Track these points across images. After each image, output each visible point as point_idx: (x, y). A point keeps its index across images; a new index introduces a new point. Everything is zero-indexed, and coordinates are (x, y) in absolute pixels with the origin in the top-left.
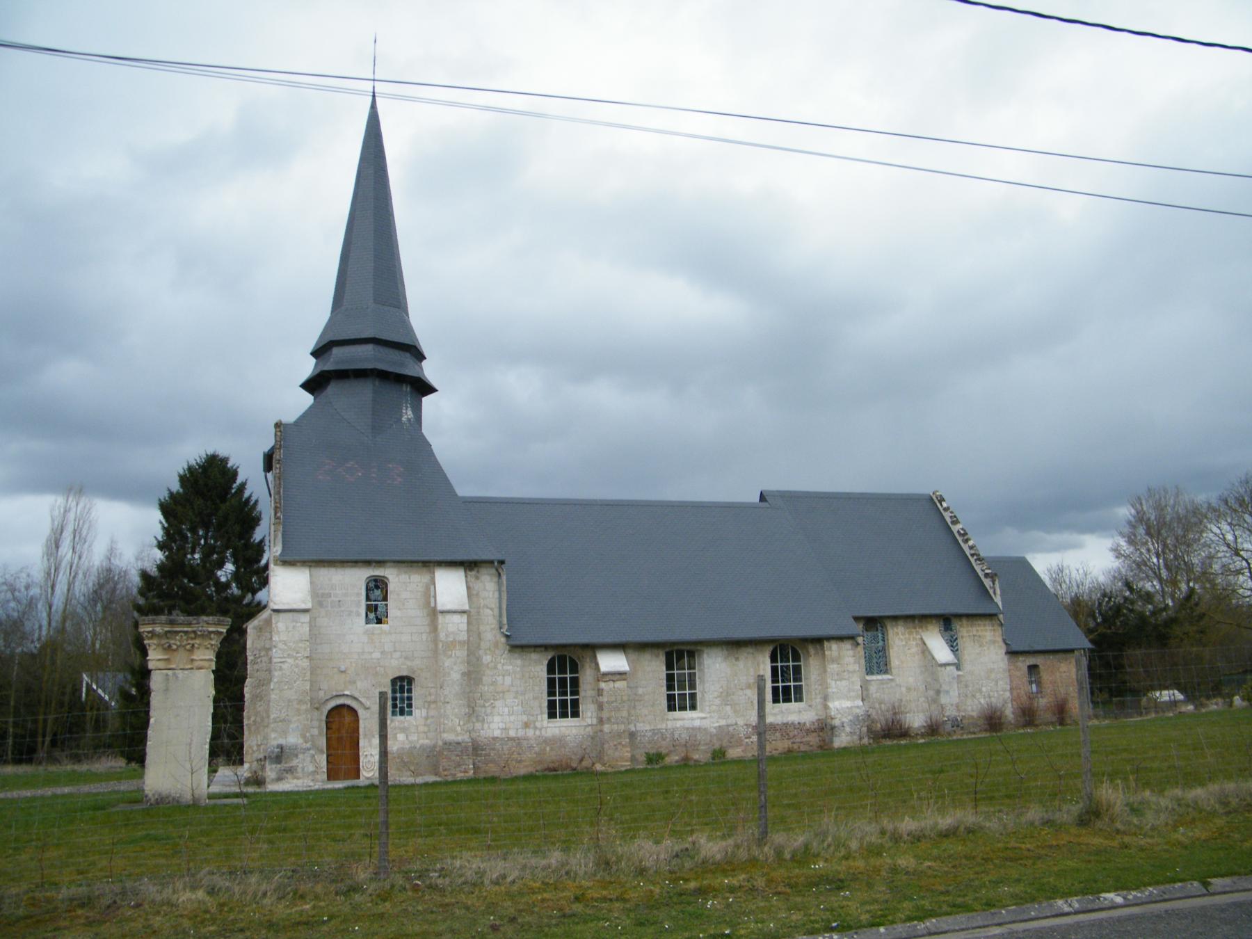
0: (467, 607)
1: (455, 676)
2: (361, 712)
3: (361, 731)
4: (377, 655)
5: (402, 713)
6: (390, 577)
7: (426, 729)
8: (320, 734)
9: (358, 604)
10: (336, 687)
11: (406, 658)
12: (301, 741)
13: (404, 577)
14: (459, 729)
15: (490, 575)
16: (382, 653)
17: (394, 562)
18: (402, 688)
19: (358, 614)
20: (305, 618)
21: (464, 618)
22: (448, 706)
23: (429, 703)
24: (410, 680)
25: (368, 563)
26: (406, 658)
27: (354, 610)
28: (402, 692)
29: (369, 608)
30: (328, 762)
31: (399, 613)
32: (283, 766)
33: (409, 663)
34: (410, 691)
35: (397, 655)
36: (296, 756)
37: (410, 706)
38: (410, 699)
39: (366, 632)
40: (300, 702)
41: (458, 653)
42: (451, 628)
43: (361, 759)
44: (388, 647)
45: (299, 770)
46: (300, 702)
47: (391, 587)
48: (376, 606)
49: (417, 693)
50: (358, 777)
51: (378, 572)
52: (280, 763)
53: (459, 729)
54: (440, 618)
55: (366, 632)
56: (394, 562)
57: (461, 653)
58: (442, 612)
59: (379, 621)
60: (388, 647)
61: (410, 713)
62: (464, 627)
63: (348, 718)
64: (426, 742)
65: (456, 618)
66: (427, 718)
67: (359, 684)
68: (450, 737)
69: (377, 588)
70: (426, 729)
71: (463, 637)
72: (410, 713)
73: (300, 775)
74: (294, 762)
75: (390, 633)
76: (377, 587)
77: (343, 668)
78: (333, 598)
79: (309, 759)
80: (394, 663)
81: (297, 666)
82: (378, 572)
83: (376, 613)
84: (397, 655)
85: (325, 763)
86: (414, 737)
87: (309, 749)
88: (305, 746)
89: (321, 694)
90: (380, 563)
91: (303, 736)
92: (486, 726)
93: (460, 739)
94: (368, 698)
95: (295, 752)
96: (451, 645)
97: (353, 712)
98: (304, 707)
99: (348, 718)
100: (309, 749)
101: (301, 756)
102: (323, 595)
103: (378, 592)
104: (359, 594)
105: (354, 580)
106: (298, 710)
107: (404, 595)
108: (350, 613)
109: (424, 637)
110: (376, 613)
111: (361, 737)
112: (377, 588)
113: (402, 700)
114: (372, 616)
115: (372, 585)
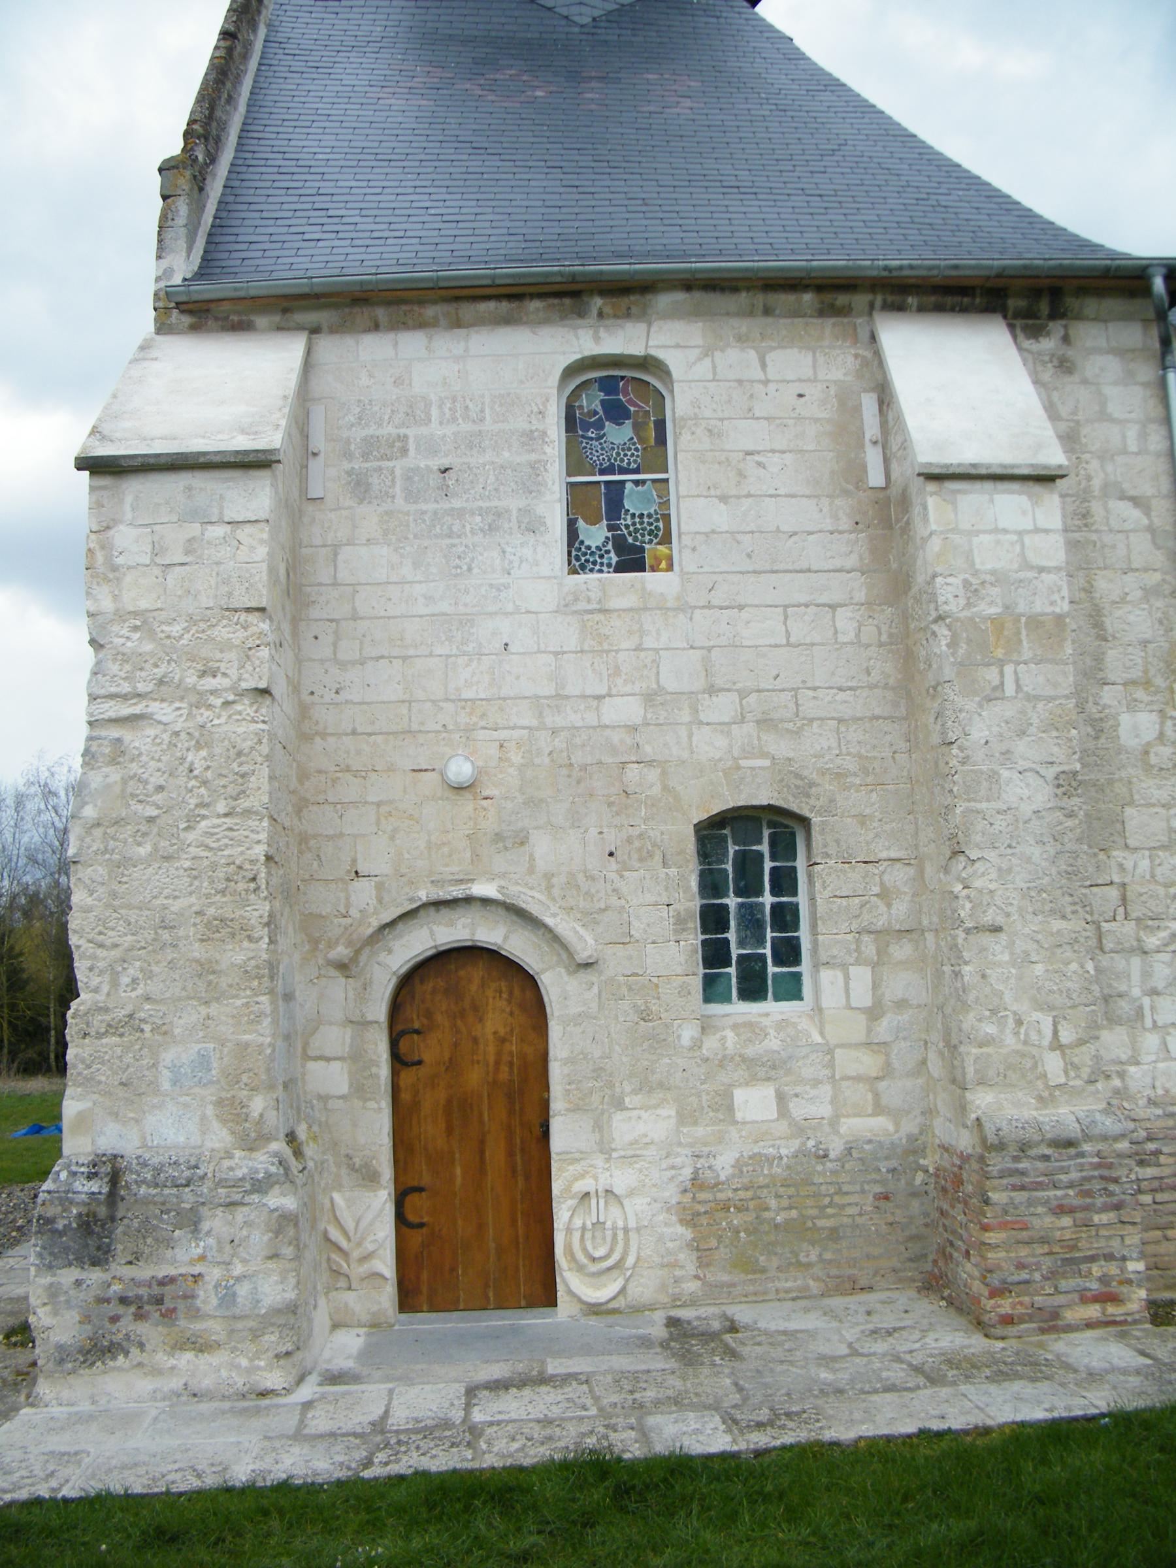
0: (1054, 457)
1: (1026, 792)
2: (555, 985)
3: (557, 1072)
4: (625, 709)
5: (753, 989)
6: (673, 360)
7: (869, 1063)
8: (359, 1090)
9: (531, 484)
10: (405, 862)
11: (766, 723)
12: (219, 1137)
13: (738, 360)
14: (1053, 1064)
15: (1120, 352)
16: (649, 698)
17: (691, 283)
18: (748, 865)
19: (533, 527)
20: (254, 498)
21: (1049, 510)
22: (997, 947)
23: (884, 936)
24: (782, 827)
25: (569, 294)
26: (766, 723)
27: (514, 504)
28: (749, 886)
29: (579, 502)
30: (401, 1218)
31: (720, 517)
32: (122, 1274)
33: (780, 747)
34: (785, 881)
35: (722, 707)
36: (191, 1221)
37: (788, 952)
38: (786, 917)
39: (567, 606)
40: (219, 929)
41: (1035, 678)
42: (990, 556)
43: (562, 1214)
44: (679, 673)
45: (207, 1298)
46: (219, 929)
47: (681, 403)
48: (615, 493)
49: (828, 894)
50: (548, 1298)
51: (622, 339)
52: (100, 1257)
53: (1053, 1064)
54: (936, 510)
55: (567, 606)
56: (691, 283)
57: (1041, 678)
58: (937, 477)
59: (631, 560)
60: (679, 673)
61: (791, 989)
62: (1051, 550)
63: (497, 1017)
64: (879, 1125)
65: (1010, 507)
66: (874, 1013)
67: (542, 847)
68: (1004, 1107)
69: (615, 407)
70: (869, 1063)
71: (1051, 596)
72: (791, 989)
73: (215, 1328)
74: (182, 1256)
75: (684, 608)
76: (616, 412)
77: (460, 769)
78: (415, 459)
79: (259, 1239)
80: (710, 746)
81: (203, 739)
82: (622, 339)
83: (617, 529)
84: (722, 707)
85: (384, 1231)
86: (814, 1105)
87: (260, 1186)
88: (243, 1164)
89: (363, 893)
90: (627, 292)
91: (232, 1111)
92: (1151, 1041)
93: (1065, 1116)
94: (590, 918)
95: (184, 1196)
96: (1001, 635)
97: (522, 983)
98: (236, 955)
99: (497, 1017)
100: (260, 1186)
101: (215, 1223)
102: (370, 446)
103: (619, 434)
104: (532, 438)
105: (521, 370)
106: (206, 969)
107: (744, 436)
108: (494, 522)
109: (846, 621)
110: (617, 529)
111: (557, 1104)
112: (615, 407)
113: (751, 922)
114: (595, 535)
115: (593, 402)
